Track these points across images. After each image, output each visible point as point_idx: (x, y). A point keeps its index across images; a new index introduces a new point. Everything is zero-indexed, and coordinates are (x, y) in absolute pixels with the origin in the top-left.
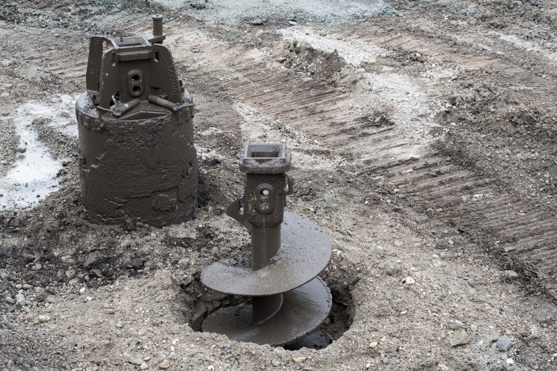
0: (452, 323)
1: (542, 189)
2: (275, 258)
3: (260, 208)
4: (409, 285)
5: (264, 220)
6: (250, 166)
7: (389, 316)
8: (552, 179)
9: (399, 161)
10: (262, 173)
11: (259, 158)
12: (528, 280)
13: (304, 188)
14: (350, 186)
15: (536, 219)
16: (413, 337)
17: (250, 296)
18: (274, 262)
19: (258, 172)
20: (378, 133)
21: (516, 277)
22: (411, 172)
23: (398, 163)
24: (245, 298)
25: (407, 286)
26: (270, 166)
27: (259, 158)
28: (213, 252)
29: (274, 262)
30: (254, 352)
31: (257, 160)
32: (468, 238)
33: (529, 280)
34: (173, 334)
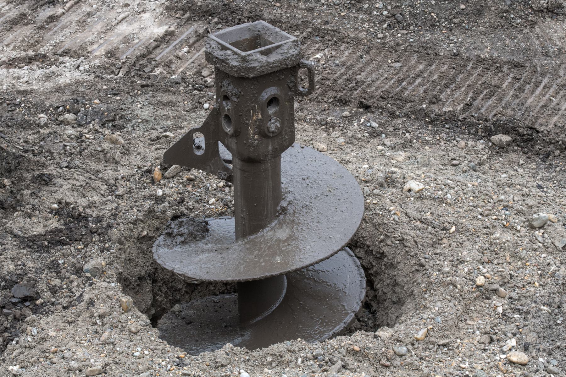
0: (536, 219)
1: (385, 26)
2: (284, 204)
3: (268, 128)
4: (418, 192)
5: (270, 148)
6: (256, 64)
7: (442, 239)
8: (389, 8)
9: (156, 40)
10: (274, 70)
11: (263, 49)
12: (530, 140)
13: (104, 111)
14: (153, 91)
15: (421, 67)
16: (507, 254)
17: (233, 282)
18: (284, 209)
19: (270, 70)
20: (67, 11)
21: (510, 141)
22: (188, 52)
23: (156, 43)
24: (227, 287)
25: (418, 195)
26: (284, 57)
27: (263, 49)
28: (115, 238)
29: (284, 209)
30: (357, 348)
31: (262, 53)
32: (382, 113)
33: (530, 140)
34: (223, 366)
